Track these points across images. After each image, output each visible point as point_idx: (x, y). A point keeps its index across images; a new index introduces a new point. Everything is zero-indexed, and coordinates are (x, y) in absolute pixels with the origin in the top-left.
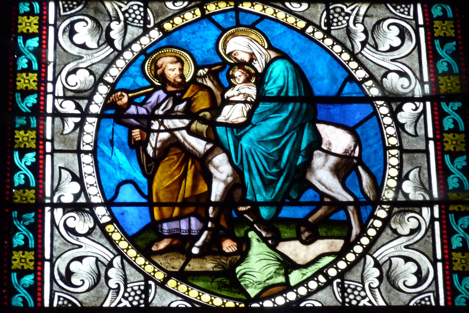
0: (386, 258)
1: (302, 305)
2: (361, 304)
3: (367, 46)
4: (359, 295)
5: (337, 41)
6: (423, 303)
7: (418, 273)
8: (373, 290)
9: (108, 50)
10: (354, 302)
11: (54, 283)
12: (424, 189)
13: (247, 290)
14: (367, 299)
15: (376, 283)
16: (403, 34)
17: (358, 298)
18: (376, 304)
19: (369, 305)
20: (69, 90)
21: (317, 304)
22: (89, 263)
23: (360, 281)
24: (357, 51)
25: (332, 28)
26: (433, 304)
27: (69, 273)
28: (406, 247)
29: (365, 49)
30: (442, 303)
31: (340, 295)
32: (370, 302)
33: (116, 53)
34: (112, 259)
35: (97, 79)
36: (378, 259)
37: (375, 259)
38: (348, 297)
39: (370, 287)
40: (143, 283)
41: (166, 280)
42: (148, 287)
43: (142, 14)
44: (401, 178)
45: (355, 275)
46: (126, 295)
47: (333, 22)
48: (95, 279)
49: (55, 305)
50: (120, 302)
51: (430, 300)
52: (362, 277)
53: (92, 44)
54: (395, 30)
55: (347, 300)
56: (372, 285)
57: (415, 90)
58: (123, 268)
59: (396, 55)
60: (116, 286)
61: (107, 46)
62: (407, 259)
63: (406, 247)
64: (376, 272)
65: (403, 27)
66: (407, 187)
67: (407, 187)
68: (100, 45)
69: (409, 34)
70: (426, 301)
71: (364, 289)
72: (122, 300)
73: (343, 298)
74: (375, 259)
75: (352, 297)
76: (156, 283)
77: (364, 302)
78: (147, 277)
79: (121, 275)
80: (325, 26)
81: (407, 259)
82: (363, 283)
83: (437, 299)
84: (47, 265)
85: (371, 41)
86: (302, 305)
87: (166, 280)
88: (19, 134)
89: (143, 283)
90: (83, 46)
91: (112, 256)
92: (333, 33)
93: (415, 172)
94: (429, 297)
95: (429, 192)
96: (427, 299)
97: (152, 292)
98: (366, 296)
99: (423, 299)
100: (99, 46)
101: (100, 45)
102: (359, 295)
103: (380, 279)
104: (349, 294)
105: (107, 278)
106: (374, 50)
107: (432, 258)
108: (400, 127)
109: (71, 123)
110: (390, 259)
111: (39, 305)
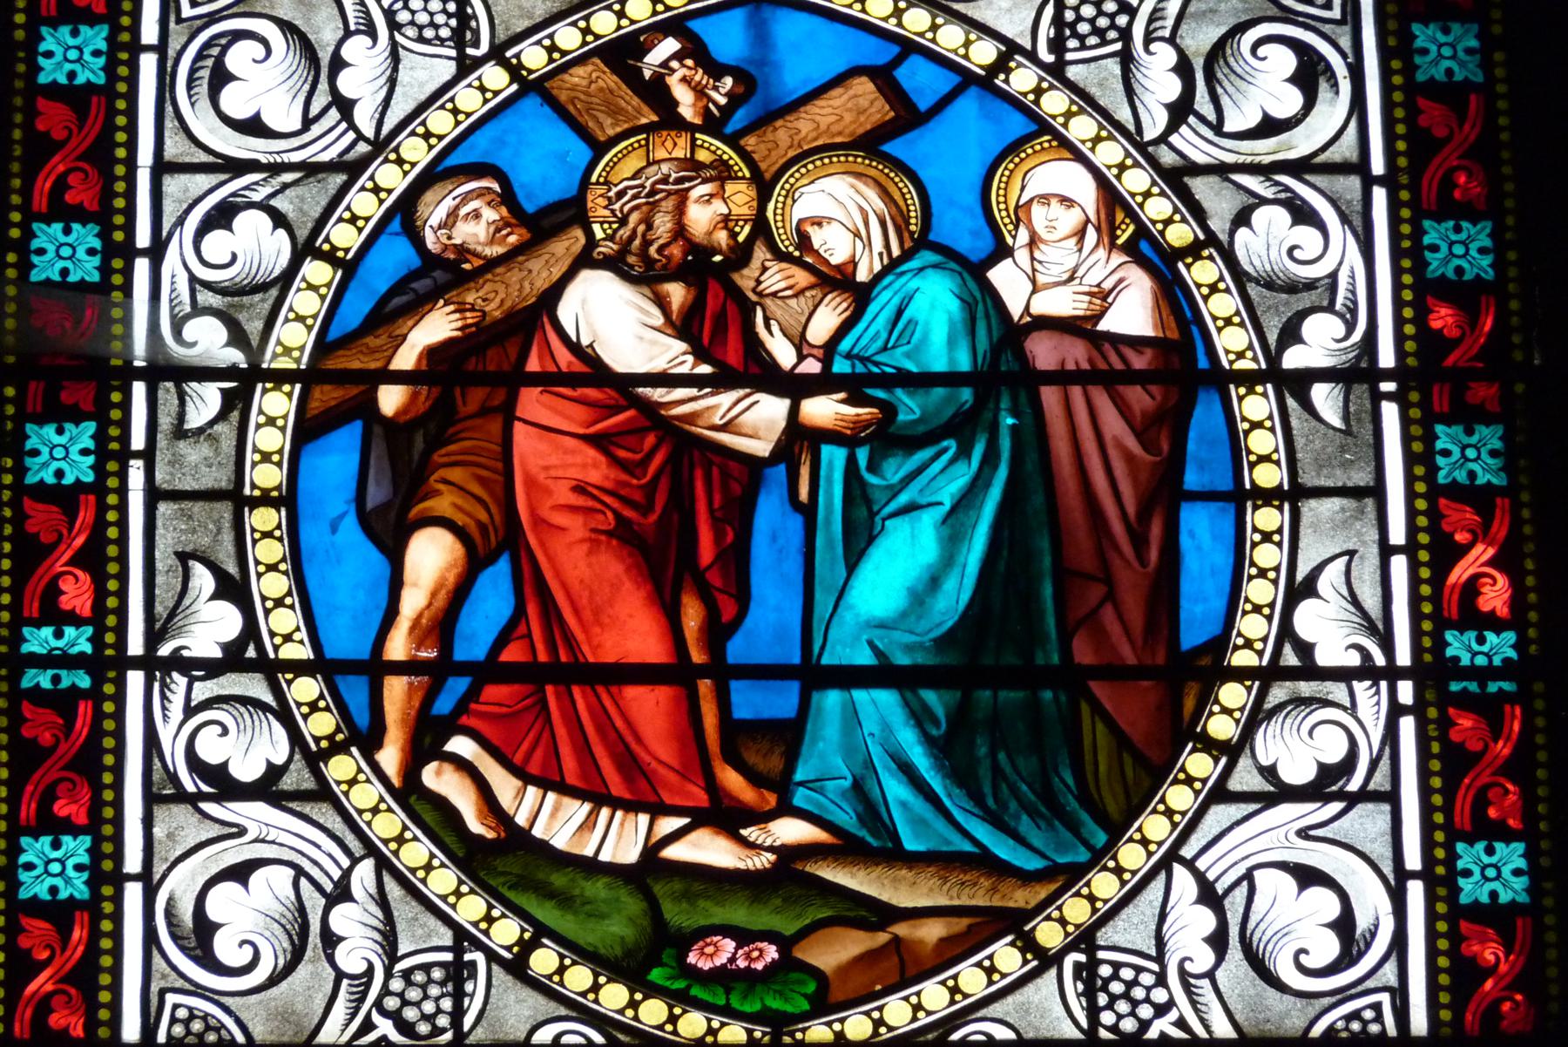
0: (1240, 870)
1: (956, 1036)
2: (1152, 1034)
3: (329, 887)
4: (1147, 1000)
5: (1085, 99)
6: (1356, 1026)
7: (1344, 925)
8: (1192, 981)
9: (1220, 865)
10: (1128, 1025)
11: (155, 952)
12: (1370, 628)
13: (756, 248)
14: (1173, 1015)
15: (1203, 958)
16: (1309, 76)
17: (1145, 1012)
18: (1201, 1032)
19: (1177, 1033)
20: (208, 285)
21: (1002, 1033)
22: (273, 884)
23: (1153, 953)
24: (1150, 134)
25: (448, 957)
26: (1392, 1031)
27: (205, 929)
28: (1303, 834)
29: (1184, 129)
30: (1419, 1023)
31: (1085, 1004)
32: (1181, 1023)
33: (1187, 852)
34: (347, 874)
35: (1248, 751)
36: (1211, 876)
37: (1200, 877)
38: (1110, 1006)
39: (1184, 975)
40: (1069, 56)
41: (1001, 65)
42: (1057, 45)
43: (1102, 999)
44: (1301, 590)
45: (1132, 930)
46: (1122, 20)
47: (442, 984)
48: (295, 937)
49: (161, 1037)
50: (368, 1026)
51: (1379, 1018)
52: (1160, 943)
53: (1274, 885)
54: (1283, 61)
55: (1107, 1018)
56: (1188, 966)
57: (181, 717)
58: (382, 901)
59: (233, 852)
60: (1153, 47)
61: (1217, 880)
62: (1307, 877)
63: (1303, 834)
64: (1206, 920)
65: (196, 960)
66: (1311, 620)
67: (1311, 620)
68: (1245, 883)
69: (1332, 81)
70: (1365, 1023)
71: (1161, 980)
72: (376, 1018)
73: (1093, 1011)
74: (1200, 877)
75: (1123, 1007)
76: (1032, 56)
77: (1163, 1026)
78: (462, 938)
79: (376, 923)
80: (473, 965)
81: (1307, 877)
82: (1160, 958)
83: (1402, 1013)
84: (133, 894)
85: (1203, 103)
86: (956, 1036)
87: (1001, 65)
88: (39, 436)
89: (1069, 56)
90: (254, 127)
91: (1174, 139)
92: (446, 937)
93: (1334, 572)
94: (1377, 1007)
95: (1387, 645)
96: (1368, 1014)
97: (1046, 30)
98: (1171, 1004)
99: (1355, 1015)
100: (1248, 876)
101: (1245, 883)
102: (1147, 1000)
103: (338, 64)
104: (1113, 998)
105: (1183, 68)
106: (1209, 134)
107: (1388, 869)
108: (233, 589)
109: (206, 401)
110: (1248, 876)
111: (103, 1033)
